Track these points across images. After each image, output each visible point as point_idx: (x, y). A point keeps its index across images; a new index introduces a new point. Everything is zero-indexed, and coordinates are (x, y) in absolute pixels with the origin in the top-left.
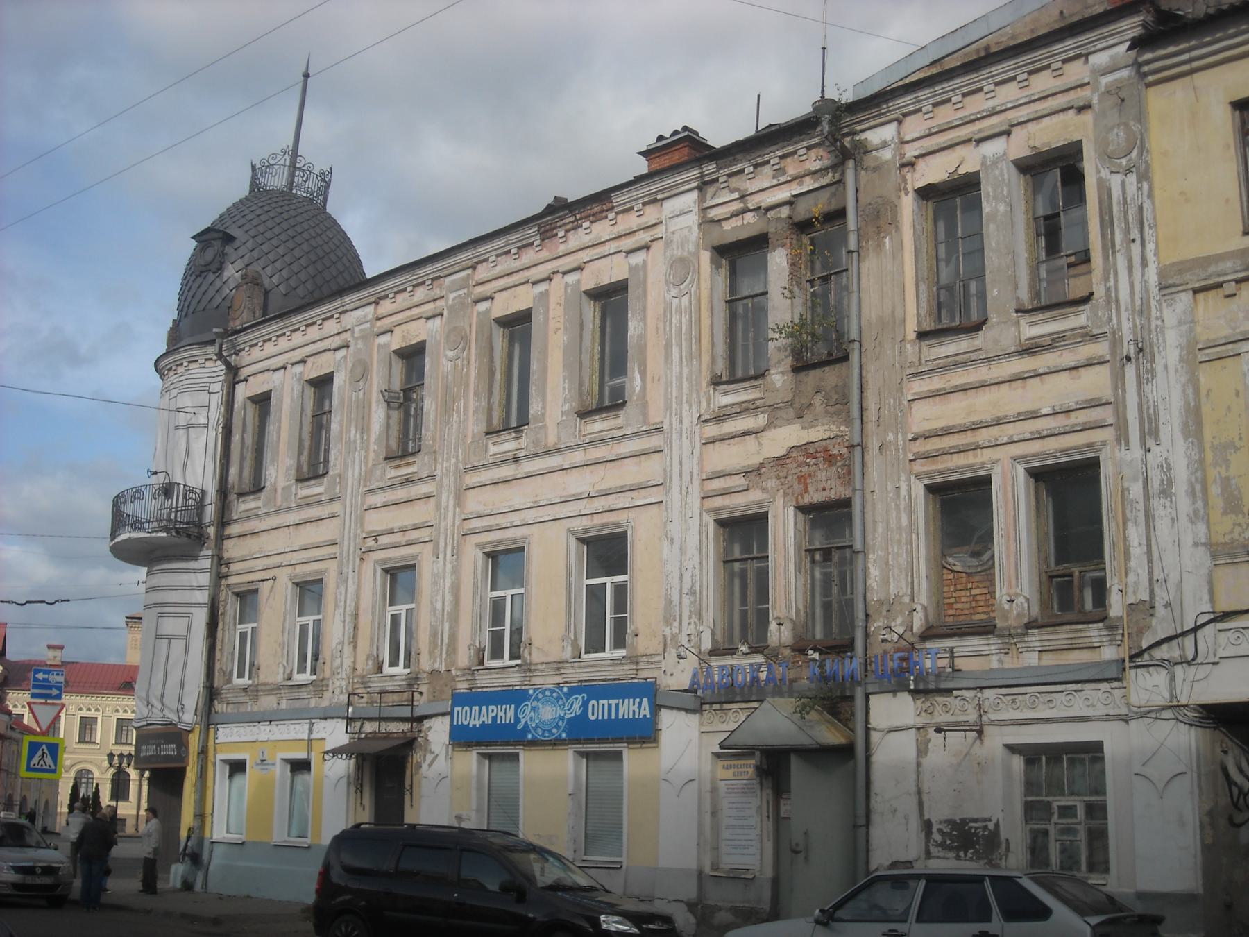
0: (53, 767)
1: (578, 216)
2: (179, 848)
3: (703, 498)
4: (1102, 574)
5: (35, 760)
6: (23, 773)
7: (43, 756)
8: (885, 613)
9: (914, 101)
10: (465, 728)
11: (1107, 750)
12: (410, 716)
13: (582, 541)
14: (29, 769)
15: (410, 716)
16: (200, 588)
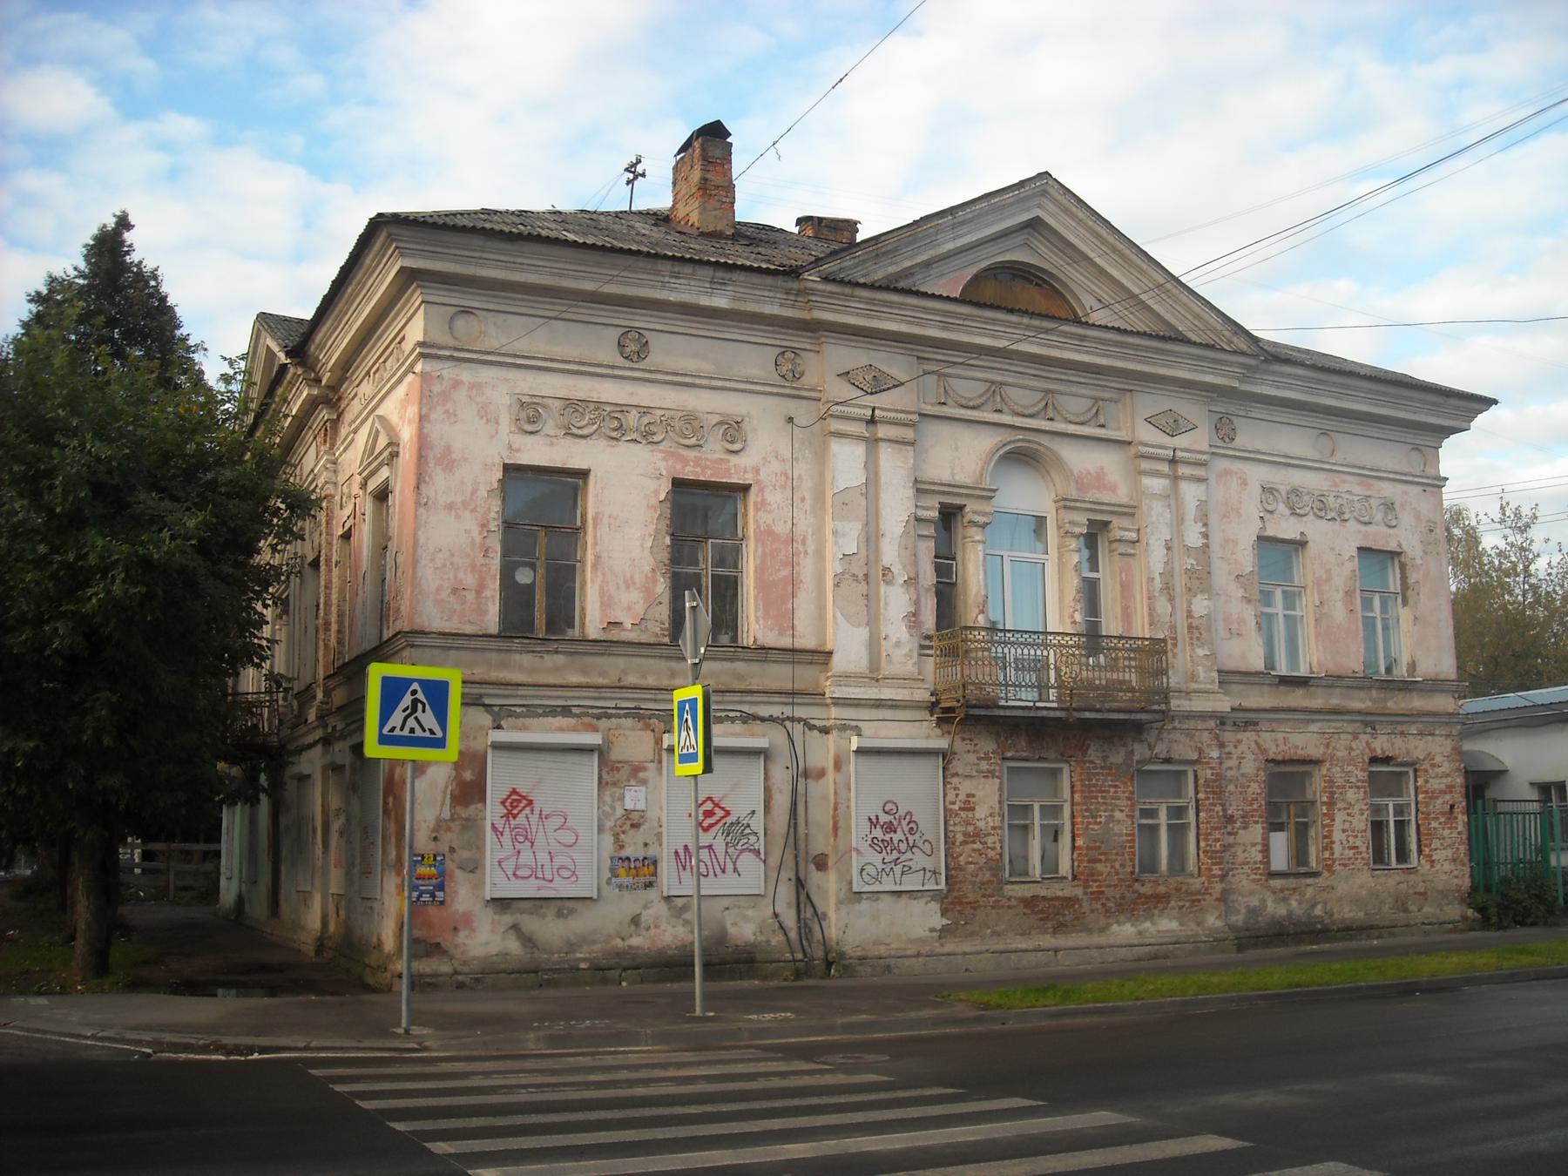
0: (439, 734)
1: (1437, 732)
2: (1247, 1147)
3: (1138, 541)
4: (1286, 612)
5: (397, 718)
6: (372, 749)
7: (414, 710)
8: (653, 931)
9: (1528, 837)
10: (421, 976)
11: (835, 659)
12: (627, 209)
13: (1056, 777)
14: (384, 740)
15: (627, 209)
16: (1127, 616)
